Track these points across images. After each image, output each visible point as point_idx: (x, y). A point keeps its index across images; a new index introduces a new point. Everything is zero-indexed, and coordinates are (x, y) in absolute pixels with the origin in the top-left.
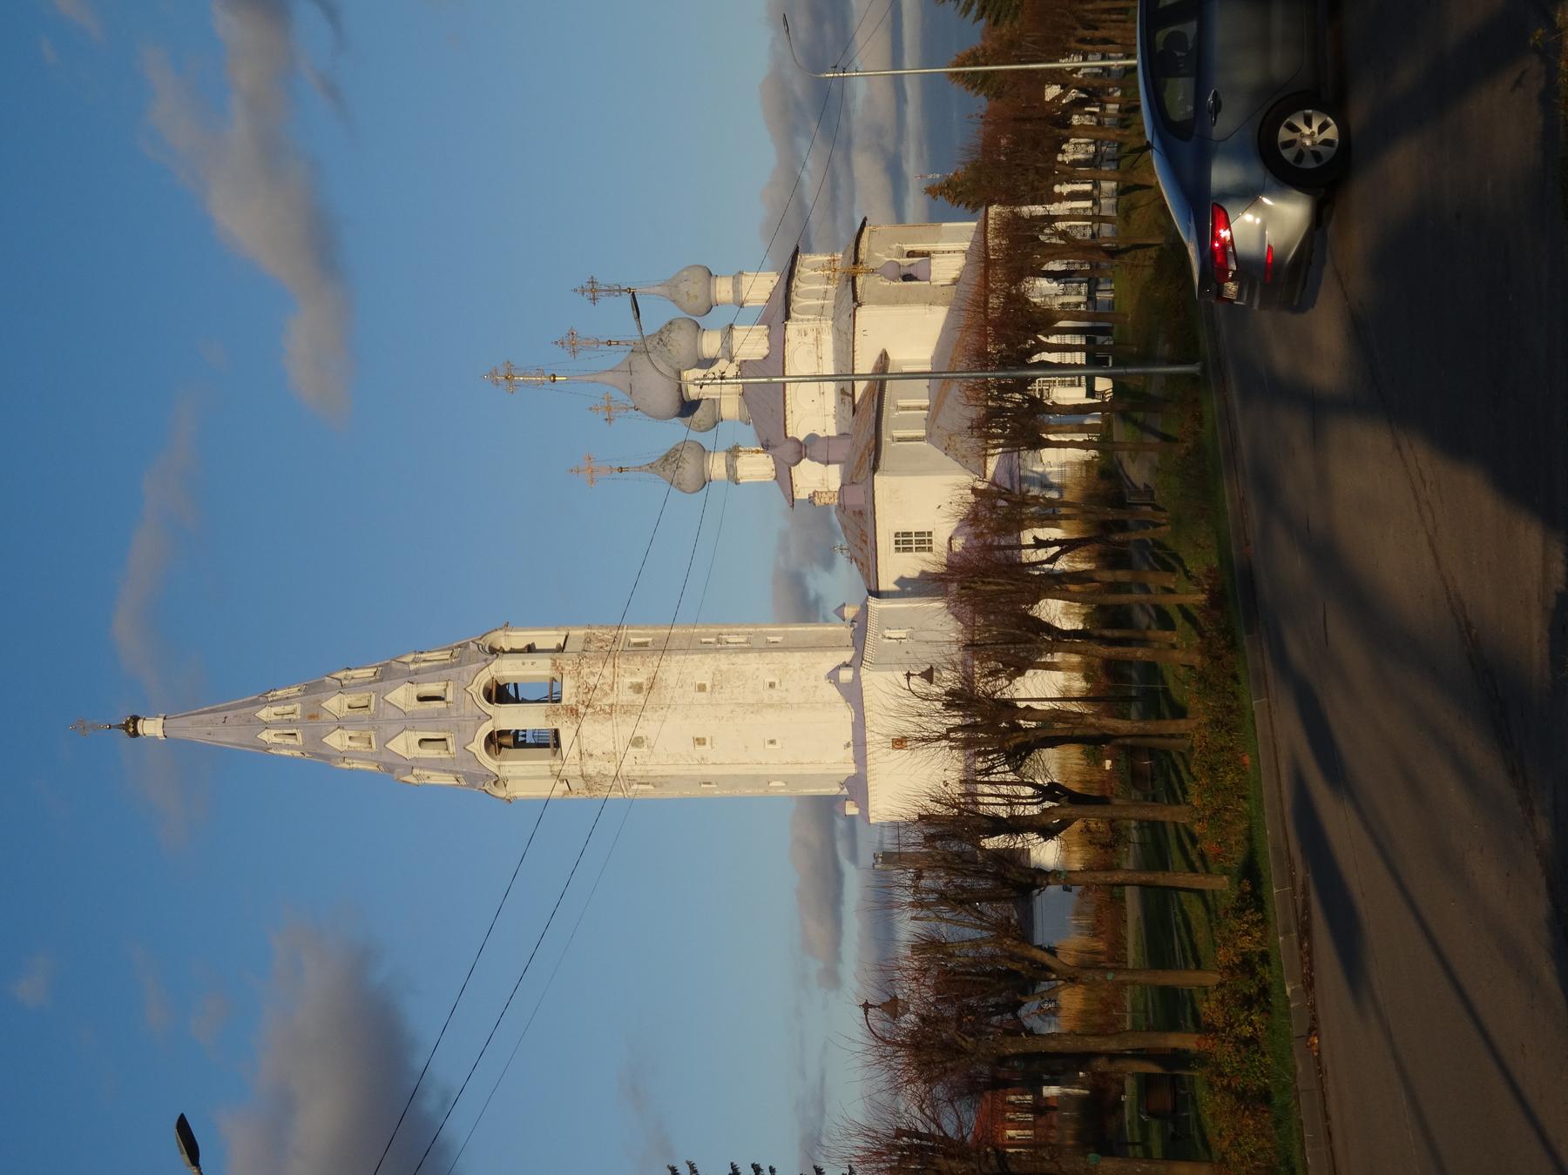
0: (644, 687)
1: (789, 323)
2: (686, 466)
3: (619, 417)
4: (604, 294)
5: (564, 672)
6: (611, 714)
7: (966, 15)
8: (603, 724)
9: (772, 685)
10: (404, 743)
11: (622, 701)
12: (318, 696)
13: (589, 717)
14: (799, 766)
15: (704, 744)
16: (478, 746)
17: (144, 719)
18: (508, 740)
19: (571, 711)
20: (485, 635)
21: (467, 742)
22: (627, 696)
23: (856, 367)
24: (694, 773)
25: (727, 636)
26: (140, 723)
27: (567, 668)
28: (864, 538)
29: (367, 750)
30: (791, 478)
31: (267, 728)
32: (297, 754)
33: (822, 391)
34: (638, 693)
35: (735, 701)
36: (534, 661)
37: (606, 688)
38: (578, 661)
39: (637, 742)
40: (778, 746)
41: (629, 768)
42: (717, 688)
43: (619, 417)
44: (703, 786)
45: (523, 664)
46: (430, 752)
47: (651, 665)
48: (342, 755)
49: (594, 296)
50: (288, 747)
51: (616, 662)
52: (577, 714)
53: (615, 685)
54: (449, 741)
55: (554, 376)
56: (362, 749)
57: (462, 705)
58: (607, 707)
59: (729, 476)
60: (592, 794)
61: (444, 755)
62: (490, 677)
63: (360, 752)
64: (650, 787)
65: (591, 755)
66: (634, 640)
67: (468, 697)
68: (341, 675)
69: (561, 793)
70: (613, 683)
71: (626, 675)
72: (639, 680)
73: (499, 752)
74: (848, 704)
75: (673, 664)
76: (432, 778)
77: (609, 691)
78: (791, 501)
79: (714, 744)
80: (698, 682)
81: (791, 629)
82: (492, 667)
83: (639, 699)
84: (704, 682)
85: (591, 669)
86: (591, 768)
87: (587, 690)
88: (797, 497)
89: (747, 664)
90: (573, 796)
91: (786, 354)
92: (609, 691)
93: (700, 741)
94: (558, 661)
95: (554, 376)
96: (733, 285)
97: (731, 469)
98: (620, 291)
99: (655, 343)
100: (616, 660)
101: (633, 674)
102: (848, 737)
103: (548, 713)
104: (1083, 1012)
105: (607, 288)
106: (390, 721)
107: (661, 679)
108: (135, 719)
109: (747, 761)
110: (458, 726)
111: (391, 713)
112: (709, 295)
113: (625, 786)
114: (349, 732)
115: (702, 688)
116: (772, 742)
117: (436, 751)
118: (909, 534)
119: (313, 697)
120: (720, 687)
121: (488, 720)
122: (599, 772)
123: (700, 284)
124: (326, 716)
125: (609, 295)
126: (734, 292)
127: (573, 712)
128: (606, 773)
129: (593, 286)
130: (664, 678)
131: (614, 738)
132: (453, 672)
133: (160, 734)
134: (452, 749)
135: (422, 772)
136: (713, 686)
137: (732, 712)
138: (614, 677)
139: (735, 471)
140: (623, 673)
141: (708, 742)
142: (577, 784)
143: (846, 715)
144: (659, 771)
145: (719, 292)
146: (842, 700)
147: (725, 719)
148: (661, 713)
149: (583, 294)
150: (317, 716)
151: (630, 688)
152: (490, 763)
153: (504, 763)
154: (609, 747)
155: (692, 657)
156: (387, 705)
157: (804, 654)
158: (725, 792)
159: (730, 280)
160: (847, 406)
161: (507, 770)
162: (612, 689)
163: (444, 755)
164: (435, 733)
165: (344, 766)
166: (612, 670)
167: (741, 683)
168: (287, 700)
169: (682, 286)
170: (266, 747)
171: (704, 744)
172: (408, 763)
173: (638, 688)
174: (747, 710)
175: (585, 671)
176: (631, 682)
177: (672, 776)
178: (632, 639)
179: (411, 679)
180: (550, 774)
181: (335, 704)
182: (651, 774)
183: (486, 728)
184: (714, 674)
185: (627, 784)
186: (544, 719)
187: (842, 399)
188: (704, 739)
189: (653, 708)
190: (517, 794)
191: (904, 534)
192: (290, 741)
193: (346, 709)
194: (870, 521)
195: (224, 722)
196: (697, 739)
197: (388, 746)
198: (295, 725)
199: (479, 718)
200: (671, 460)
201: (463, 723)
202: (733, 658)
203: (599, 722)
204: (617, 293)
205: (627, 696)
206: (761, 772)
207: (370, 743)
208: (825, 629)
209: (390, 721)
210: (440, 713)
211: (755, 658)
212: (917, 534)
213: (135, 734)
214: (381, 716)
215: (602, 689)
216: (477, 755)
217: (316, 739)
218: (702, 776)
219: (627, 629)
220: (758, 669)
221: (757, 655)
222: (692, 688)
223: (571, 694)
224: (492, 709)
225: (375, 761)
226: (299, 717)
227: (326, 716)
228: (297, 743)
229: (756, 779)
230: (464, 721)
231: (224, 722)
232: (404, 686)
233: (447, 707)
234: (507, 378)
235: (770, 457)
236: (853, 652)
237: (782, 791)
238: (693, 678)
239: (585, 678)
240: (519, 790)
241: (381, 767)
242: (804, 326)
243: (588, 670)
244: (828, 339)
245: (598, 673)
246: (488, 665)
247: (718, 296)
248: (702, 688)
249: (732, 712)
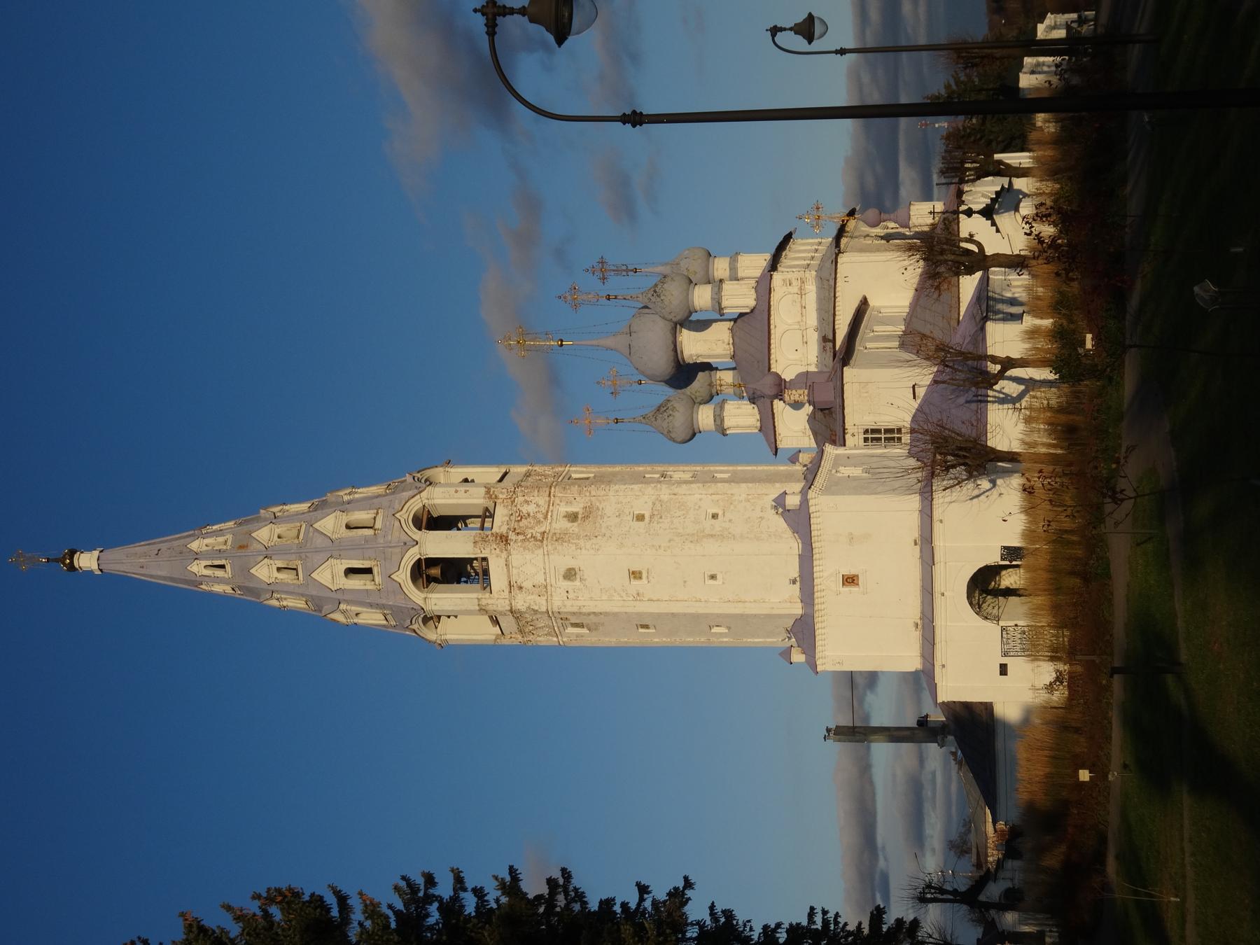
0: (580, 516)
1: (775, 273)
2: (676, 414)
3: (623, 390)
4: (612, 273)
5: (498, 501)
6: (542, 541)
9: (715, 516)
10: (330, 573)
11: (555, 529)
12: (250, 527)
14: (740, 605)
15: (641, 578)
16: (403, 575)
17: (82, 552)
18: (435, 572)
19: (501, 538)
20: (423, 470)
21: (392, 572)
23: (837, 313)
24: (628, 610)
25: (672, 473)
26: (76, 556)
27: (501, 496)
28: (833, 438)
29: (295, 582)
30: (775, 427)
31: (196, 559)
32: (228, 589)
33: (805, 340)
34: (573, 521)
35: (674, 530)
36: (468, 489)
37: (540, 516)
38: (512, 490)
39: (570, 574)
40: (718, 582)
41: (560, 603)
43: (623, 390)
44: (641, 630)
45: (456, 492)
46: (357, 583)
47: (588, 494)
49: (603, 275)
51: (552, 491)
52: (507, 541)
53: (550, 514)
54: (375, 571)
55: (562, 341)
56: (289, 581)
59: (716, 425)
60: (525, 639)
61: (370, 586)
62: (421, 505)
63: (288, 584)
64: (585, 631)
65: (521, 588)
66: (574, 476)
67: (397, 523)
68: (276, 509)
69: (494, 637)
70: (547, 512)
71: (562, 504)
72: (575, 510)
73: (427, 587)
74: (795, 534)
75: (611, 493)
76: (361, 616)
77: (542, 520)
78: (774, 450)
79: (650, 578)
81: (739, 468)
82: (424, 494)
83: (573, 527)
84: (642, 512)
85: (526, 497)
86: (521, 603)
87: (519, 518)
88: (780, 445)
89: (690, 494)
90: (505, 641)
91: (772, 303)
92: (542, 520)
93: (636, 575)
94: (492, 490)
95: (562, 341)
96: (730, 264)
97: (719, 418)
98: (627, 270)
99: (650, 295)
100: (553, 488)
101: (568, 503)
102: (795, 573)
103: (477, 539)
104: (1047, 776)
105: (615, 268)
107: (598, 509)
109: (686, 598)
111: (319, 542)
112: (707, 271)
113: (558, 627)
114: (276, 562)
115: (640, 518)
116: (713, 577)
117: (362, 582)
118: (878, 431)
119: (245, 528)
120: (659, 516)
122: (529, 607)
123: (700, 261)
125: (617, 275)
126: (730, 269)
127: (504, 539)
128: (536, 608)
129: (603, 266)
130: (601, 508)
131: (544, 569)
132: (385, 501)
133: (95, 567)
134: (378, 579)
135: (349, 608)
136: (652, 516)
137: (670, 541)
138: (549, 506)
139: (722, 420)
140: (558, 502)
141: (644, 575)
142: (508, 623)
143: (792, 546)
144: (590, 607)
145: (717, 270)
146: (789, 533)
147: (663, 549)
148: (594, 541)
149: (594, 274)
150: (247, 546)
151: (565, 517)
152: (416, 595)
153: (430, 595)
154: (540, 579)
155: (633, 486)
157: (750, 485)
158: (664, 639)
159: (728, 260)
160: (828, 353)
161: (433, 603)
162: (546, 517)
164: (361, 562)
165: (274, 603)
166: (547, 499)
167: (683, 512)
169: (682, 263)
170: (197, 581)
171: (641, 578)
172: (333, 595)
173: (573, 517)
174: (686, 539)
175: (520, 499)
176: (566, 512)
177: (606, 614)
178: (573, 475)
179: (342, 508)
180: (477, 608)
181: (264, 534)
182: (584, 610)
184: (654, 504)
185: (560, 625)
186: (472, 545)
187: (824, 347)
188: (640, 573)
189: (586, 536)
190: (448, 637)
191: (874, 431)
192: (219, 573)
193: (276, 538)
194: (839, 417)
196: (633, 573)
197: (314, 575)
198: (225, 555)
199: (405, 544)
200: (663, 409)
201: (390, 550)
202: (676, 489)
203: (528, 549)
204: (624, 273)
205: (563, 524)
206: (701, 611)
207: (297, 575)
208: (776, 468)
209: (317, 551)
210: (367, 539)
211: (699, 488)
212: (887, 431)
214: (308, 545)
215: (535, 517)
216: (402, 585)
218: (637, 614)
219: (570, 467)
220: (700, 500)
221: (701, 485)
222: (630, 518)
224: (417, 535)
225: (303, 595)
226: (229, 548)
228: (226, 576)
229: (696, 620)
230: (390, 547)
233: (375, 534)
234: (519, 342)
235: (756, 408)
236: (803, 484)
237: (725, 640)
238: (632, 507)
239: (518, 506)
240: (451, 632)
241: (309, 603)
242: (789, 276)
243: (523, 499)
244: (812, 289)
245: (534, 503)
246: (420, 492)
247: (716, 274)
248: (640, 518)
249: (670, 541)
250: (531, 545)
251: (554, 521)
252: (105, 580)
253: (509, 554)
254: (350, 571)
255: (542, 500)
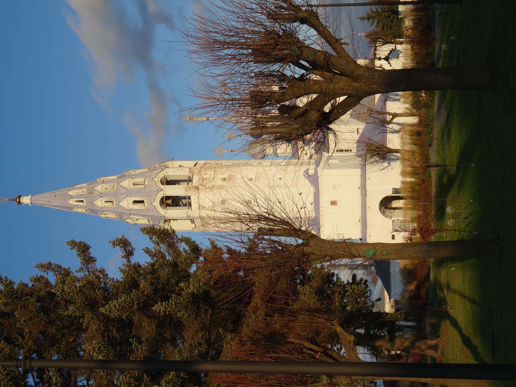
0: (227, 179)
5: (194, 174)
7: (371, 26)
8: (209, 193)
9: (280, 179)
13: (203, 190)
18: (169, 202)
19: (196, 187)
22: (220, 182)
26: (21, 198)
27: (195, 172)
32: (84, 211)
34: (224, 181)
37: (211, 179)
38: (200, 169)
42: (257, 179)
45: (177, 170)
46: (138, 206)
47: (230, 171)
48: (102, 209)
50: (80, 207)
53: (215, 178)
54: (145, 202)
57: (151, 186)
58: (211, 186)
61: (143, 208)
62: (163, 175)
67: (154, 183)
69: (192, 228)
70: (214, 178)
72: (225, 177)
80: (249, 177)
84: (252, 177)
86: (204, 213)
95: (208, 118)
101: (222, 174)
106: (122, 194)
107: (234, 176)
108: (20, 197)
110: (149, 194)
111: (122, 190)
114: (105, 199)
119: (91, 186)
121: (161, 191)
124: (96, 192)
127: (197, 188)
130: (235, 176)
136: (256, 179)
138: (215, 175)
142: (198, 222)
151: (221, 179)
152: (162, 211)
156: (121, 187)
162: (213, 180)
163: (143, 208)
164: (139, 198)
165: (103, 216)
168: (81, 188)
170: (71, 207)
172: (128, 212)
173: (224, 180)
180: (186, 216)
183: (160, 195)
184: (256, 174)
186: (184, 191)
192: (81, 204)
195: (55, 197)
199: (158, 190)
201: (151, 193)
205: (220, 182)
213: (20, 203)
214: (118, 192)
217: (92, 203)
223: (196, 182)
227: (96, 192)
228: (84, 205)
230: (151, 192)
231: (55, 197)
232: (128, 179)
234: (190, 118)
239: (202, 176)
246: (163, 170)
250: (208, 190)
251: (217, 181)
252: (33, 206)
253: (199, 194)
254: (136, 202)
255: (212, 173)
